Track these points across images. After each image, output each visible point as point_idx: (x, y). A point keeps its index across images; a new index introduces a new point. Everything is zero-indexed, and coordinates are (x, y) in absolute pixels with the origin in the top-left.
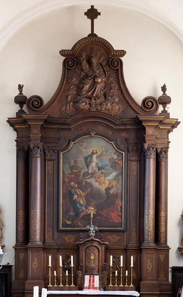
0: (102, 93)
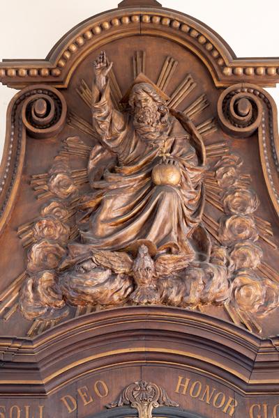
0: (186, 230)
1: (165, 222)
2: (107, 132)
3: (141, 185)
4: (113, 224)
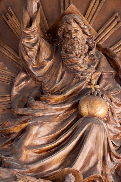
0: (110, 165)
1: (91, 154)
2: (34, 60)
3: (66, 115)
4: (38, 151)
